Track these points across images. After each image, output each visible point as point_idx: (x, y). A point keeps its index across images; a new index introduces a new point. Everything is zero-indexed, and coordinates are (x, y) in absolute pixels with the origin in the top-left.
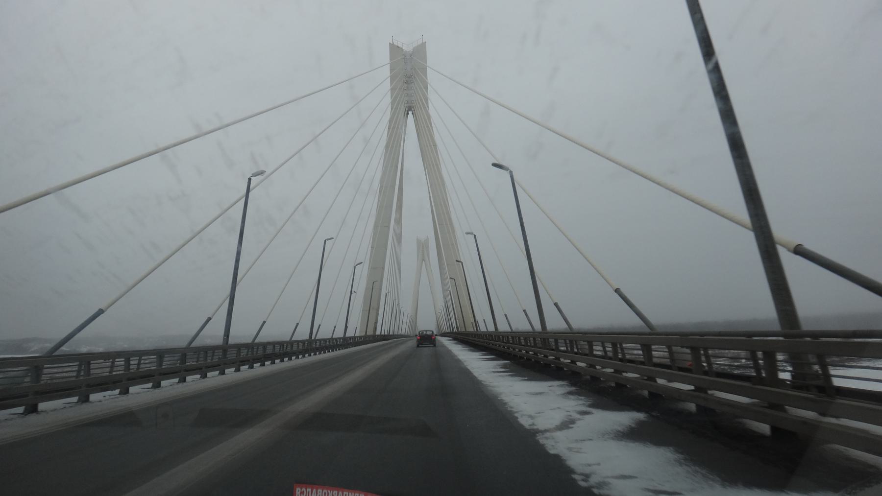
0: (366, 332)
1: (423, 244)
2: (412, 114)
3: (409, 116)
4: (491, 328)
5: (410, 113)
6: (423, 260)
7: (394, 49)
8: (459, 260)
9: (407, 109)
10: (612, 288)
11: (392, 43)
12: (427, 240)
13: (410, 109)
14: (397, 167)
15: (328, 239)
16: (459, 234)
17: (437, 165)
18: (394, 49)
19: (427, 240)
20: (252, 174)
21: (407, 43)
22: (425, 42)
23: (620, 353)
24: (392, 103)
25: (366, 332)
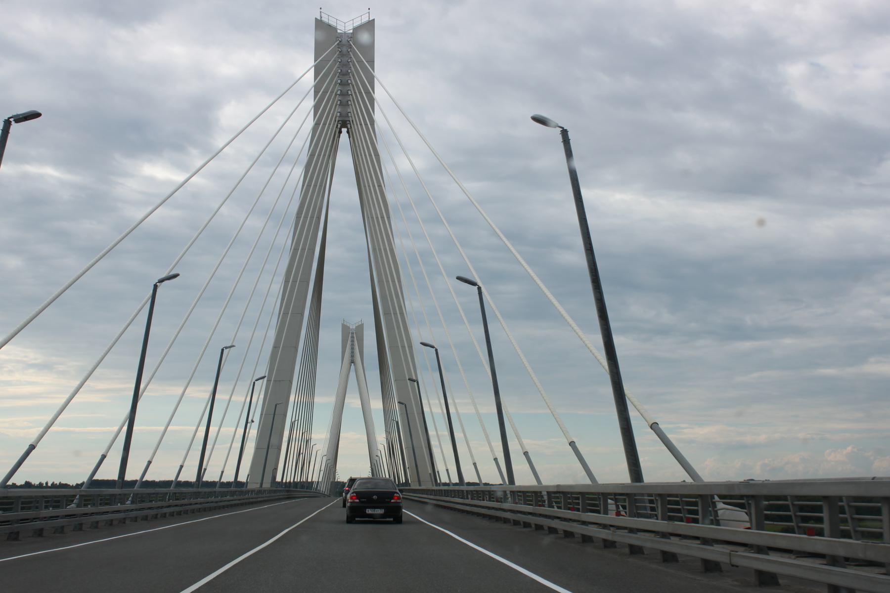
0: (262, 484)
1: (352, 333)
2: (348, 132)
3: (341, 135)
4: (455, 479)
5: (344, 130)
6: (353, 361)
8: (414, 378)
9: (339, 126)
10: (522, 449)
11: (319, 18)
12: (360, 328)
13: (344, 124)
14: (319, 218)
15: (226, 348)
16: (417, 346)
17: (380, 186)
19: (360, 328)
20: (159, 280)
21: (345, 23)
22: (374, 20)
23: (622, 511)
24: (316, 108)
25: (262, 484)
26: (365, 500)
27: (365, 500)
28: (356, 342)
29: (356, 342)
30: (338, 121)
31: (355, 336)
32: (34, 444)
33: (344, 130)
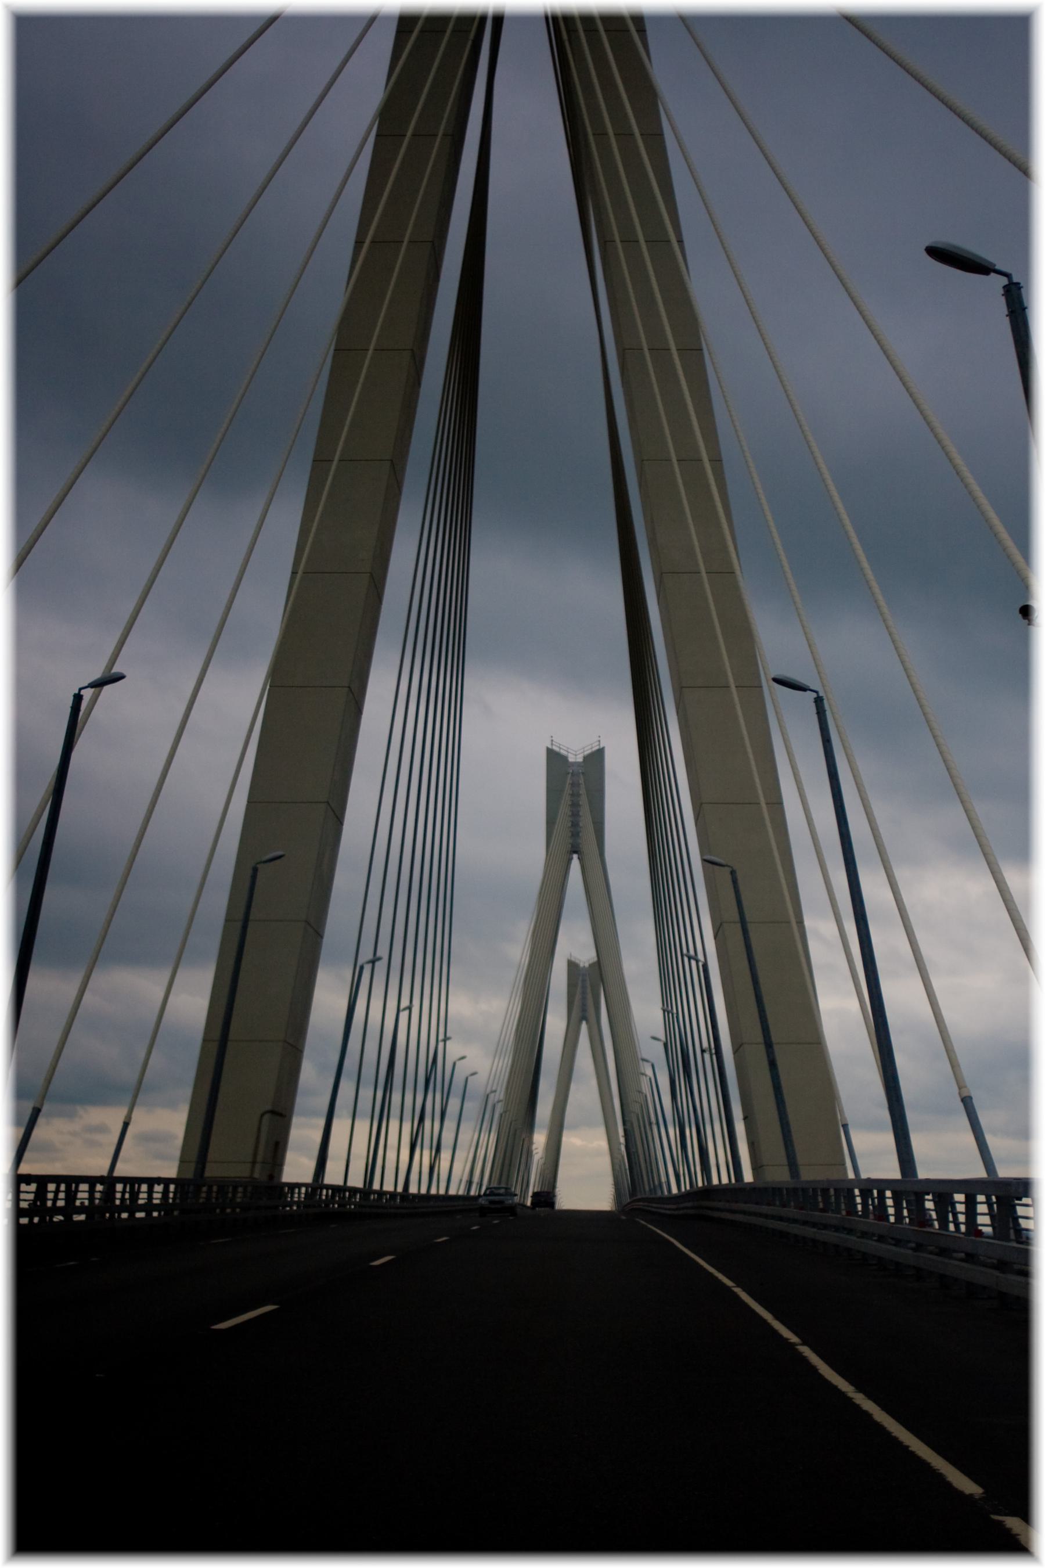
2: (579, 858)
5: (575, 856)
7: (555, 759)
11: (550, 747)
13: (575, 852)
18: (555, 759)
26: (97, 1375)
27: (97, 1375)
28: (589, 990)
29: (589, 990)
30: (571, 851)
31: (583, 791)
32: (36, 1106)
33: (575, 863)
